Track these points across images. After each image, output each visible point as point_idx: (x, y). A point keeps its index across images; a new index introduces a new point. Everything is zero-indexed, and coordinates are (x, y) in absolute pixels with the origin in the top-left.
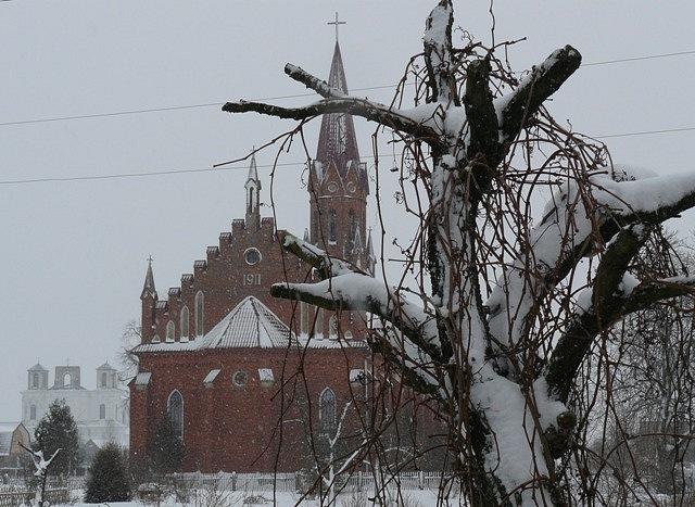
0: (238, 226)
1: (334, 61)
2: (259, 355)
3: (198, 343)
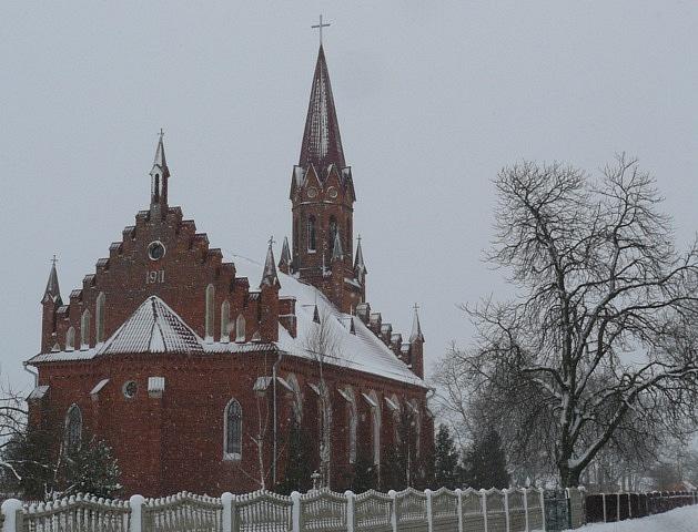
0: (143, 219)
1: (317, 75)
2: (146, 361)
3: (87, 353)
